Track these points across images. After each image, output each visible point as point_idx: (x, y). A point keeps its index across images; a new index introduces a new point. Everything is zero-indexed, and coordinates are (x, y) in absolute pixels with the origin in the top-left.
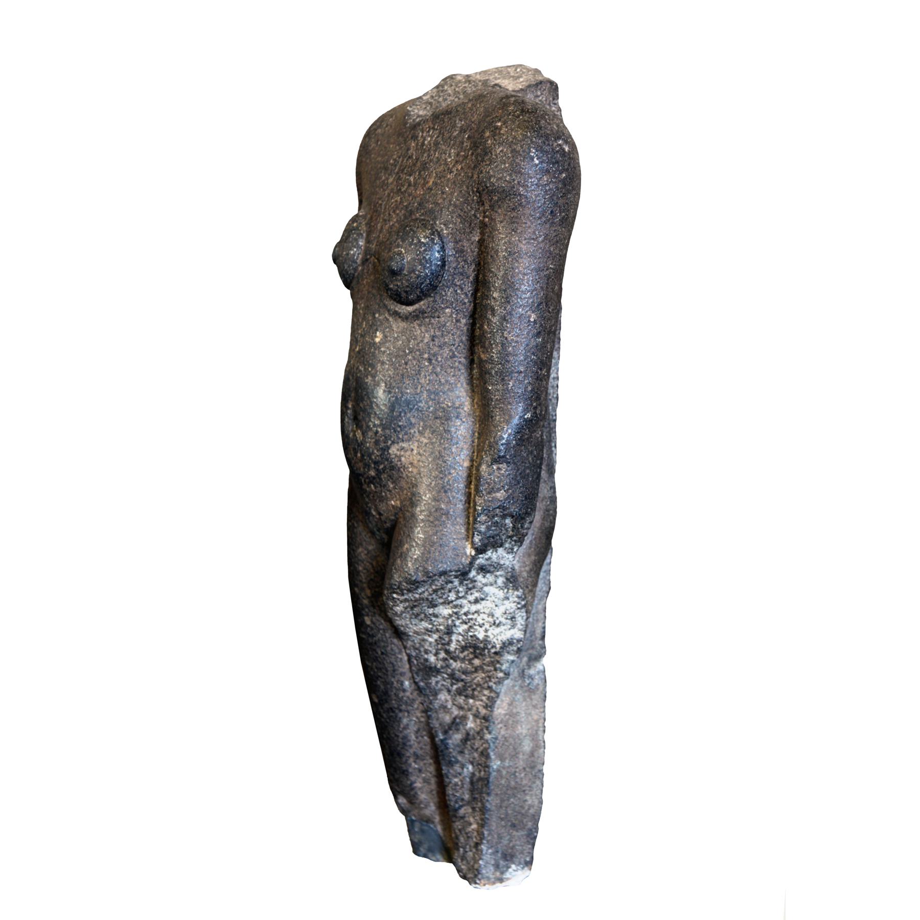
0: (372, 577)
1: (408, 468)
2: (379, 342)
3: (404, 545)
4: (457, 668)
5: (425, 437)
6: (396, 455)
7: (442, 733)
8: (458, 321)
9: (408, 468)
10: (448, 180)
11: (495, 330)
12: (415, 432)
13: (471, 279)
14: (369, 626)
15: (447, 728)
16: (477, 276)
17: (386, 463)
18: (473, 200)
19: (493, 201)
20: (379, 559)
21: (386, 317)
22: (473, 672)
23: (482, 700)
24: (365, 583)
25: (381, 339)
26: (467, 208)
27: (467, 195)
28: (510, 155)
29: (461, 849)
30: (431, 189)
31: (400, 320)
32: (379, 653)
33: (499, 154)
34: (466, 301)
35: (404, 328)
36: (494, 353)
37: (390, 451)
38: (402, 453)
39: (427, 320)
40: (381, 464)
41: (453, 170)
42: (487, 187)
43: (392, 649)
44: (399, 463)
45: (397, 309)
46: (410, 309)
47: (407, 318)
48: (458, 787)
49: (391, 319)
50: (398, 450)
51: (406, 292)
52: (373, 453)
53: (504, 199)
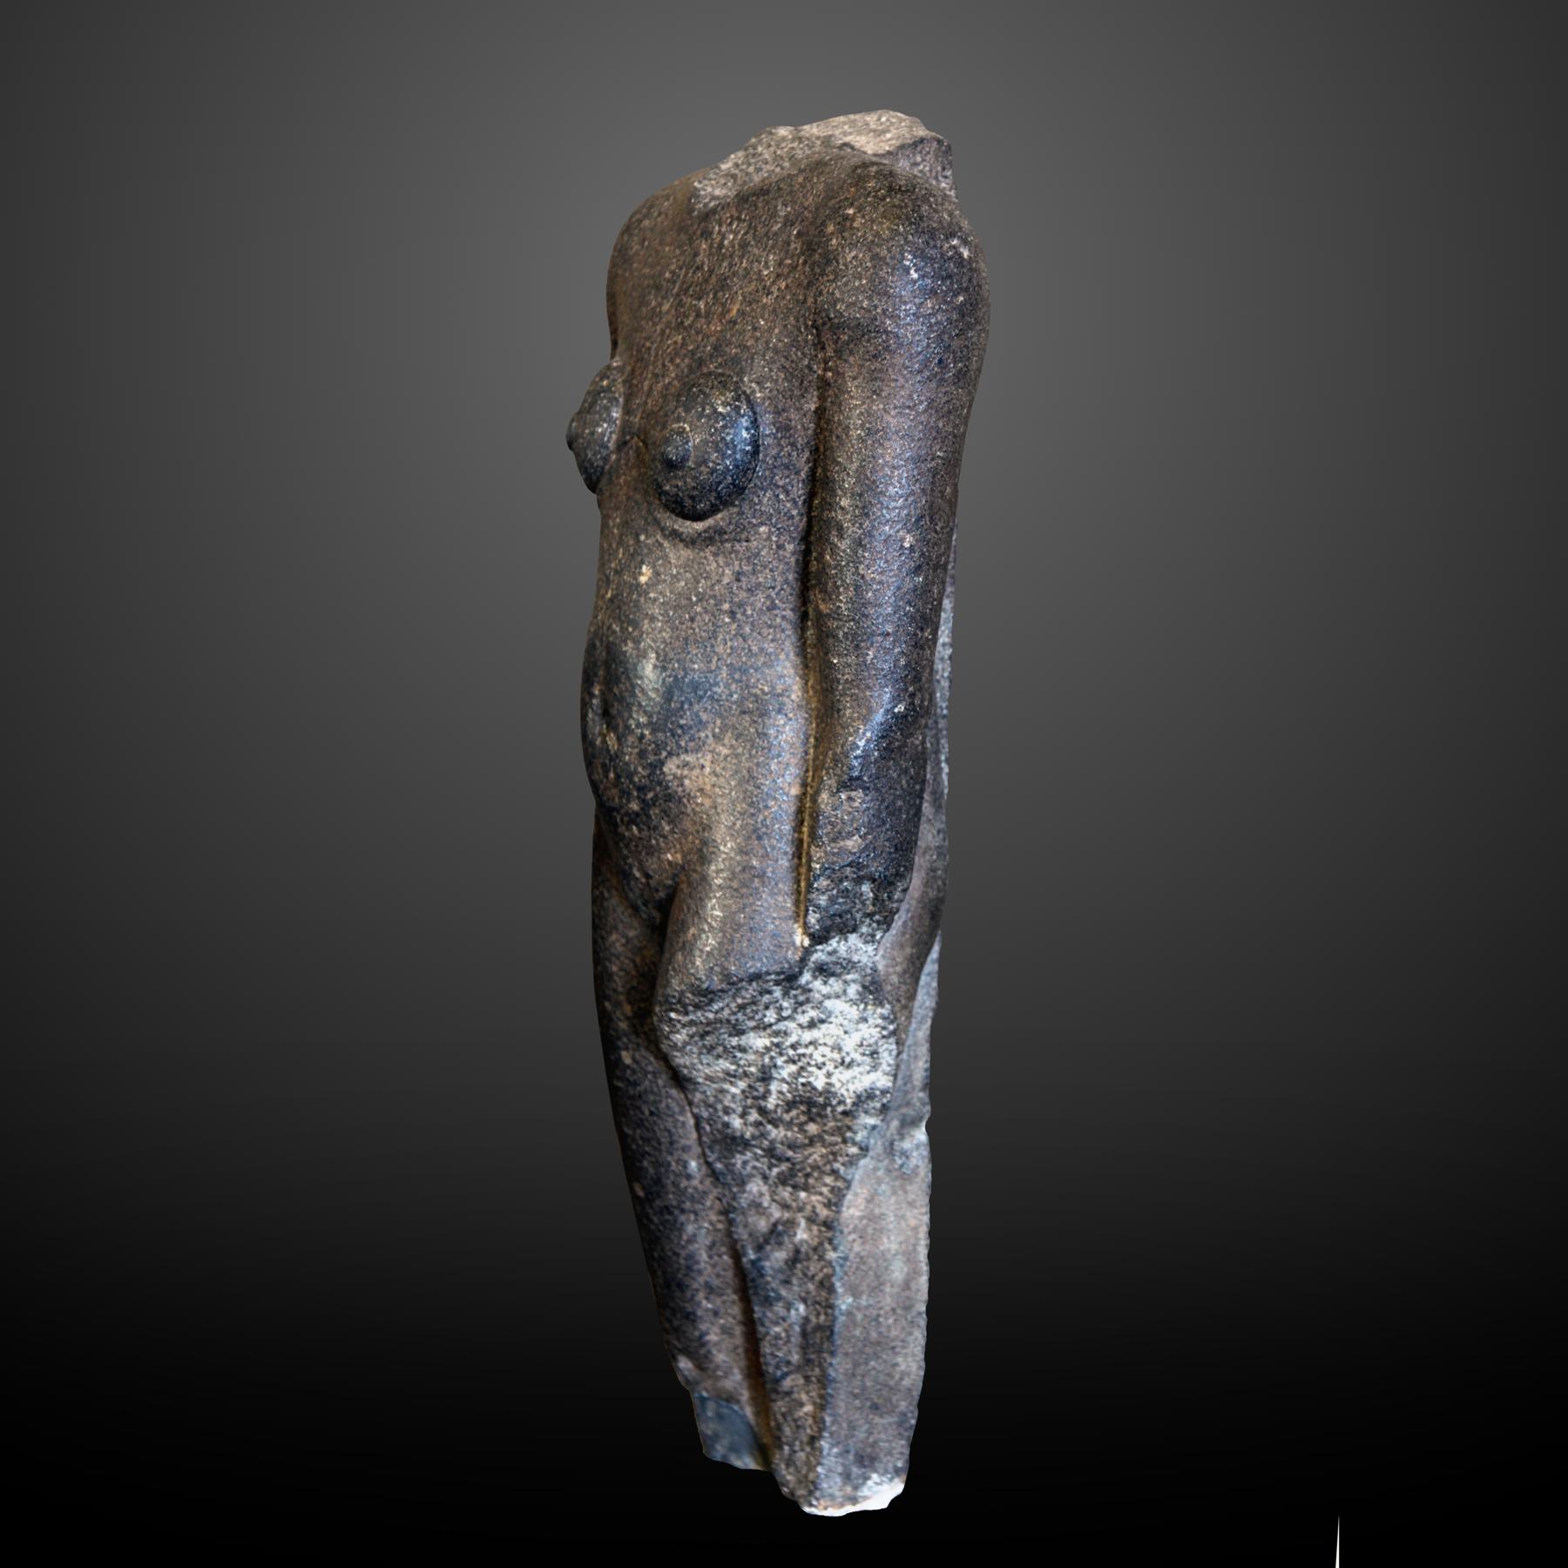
0: (635, 983)
1: (696, 797)
3: (689, 928)
4: (779, 1139)
5: (724, 745)
6: (675, 776)
7: (753, 1249)
10: (764, 307)
11: (843, 563)
12: (707, 736)
13: (803, 475)
14: (628, 1067)
15: (761, 1240)
16: (813, 471)
17: (658, 789)
18: (806, 341)
19: (840, 342)
21: (657, 541)
22: (806, 1145)
23: (821, 1194)
24: (621, 993)
25: (650, 579)
26: (796, 355)
27: (796, 332)
28: (868, 264)
29: (786, 1448)
31: (681, 545)
32: (647, 1112)
33: (851, 262)
34: (795, 512)
35: (688, 560)
36: (841, 601)
37: (665, 769)
38: (686, 772)
39: (728, 545)
40: (650, 791)
41: (773, 289)
42: (830, 319)
43: (668, 1107)
44: (680, 789)
45: (676, 527)
46: (699, 526)
47: (693, 542)
48: (780, 1342)
49: (666, 544)
50: (678, 767)
51: (692, 498)
52: (636, 772)
53: (860, 340)
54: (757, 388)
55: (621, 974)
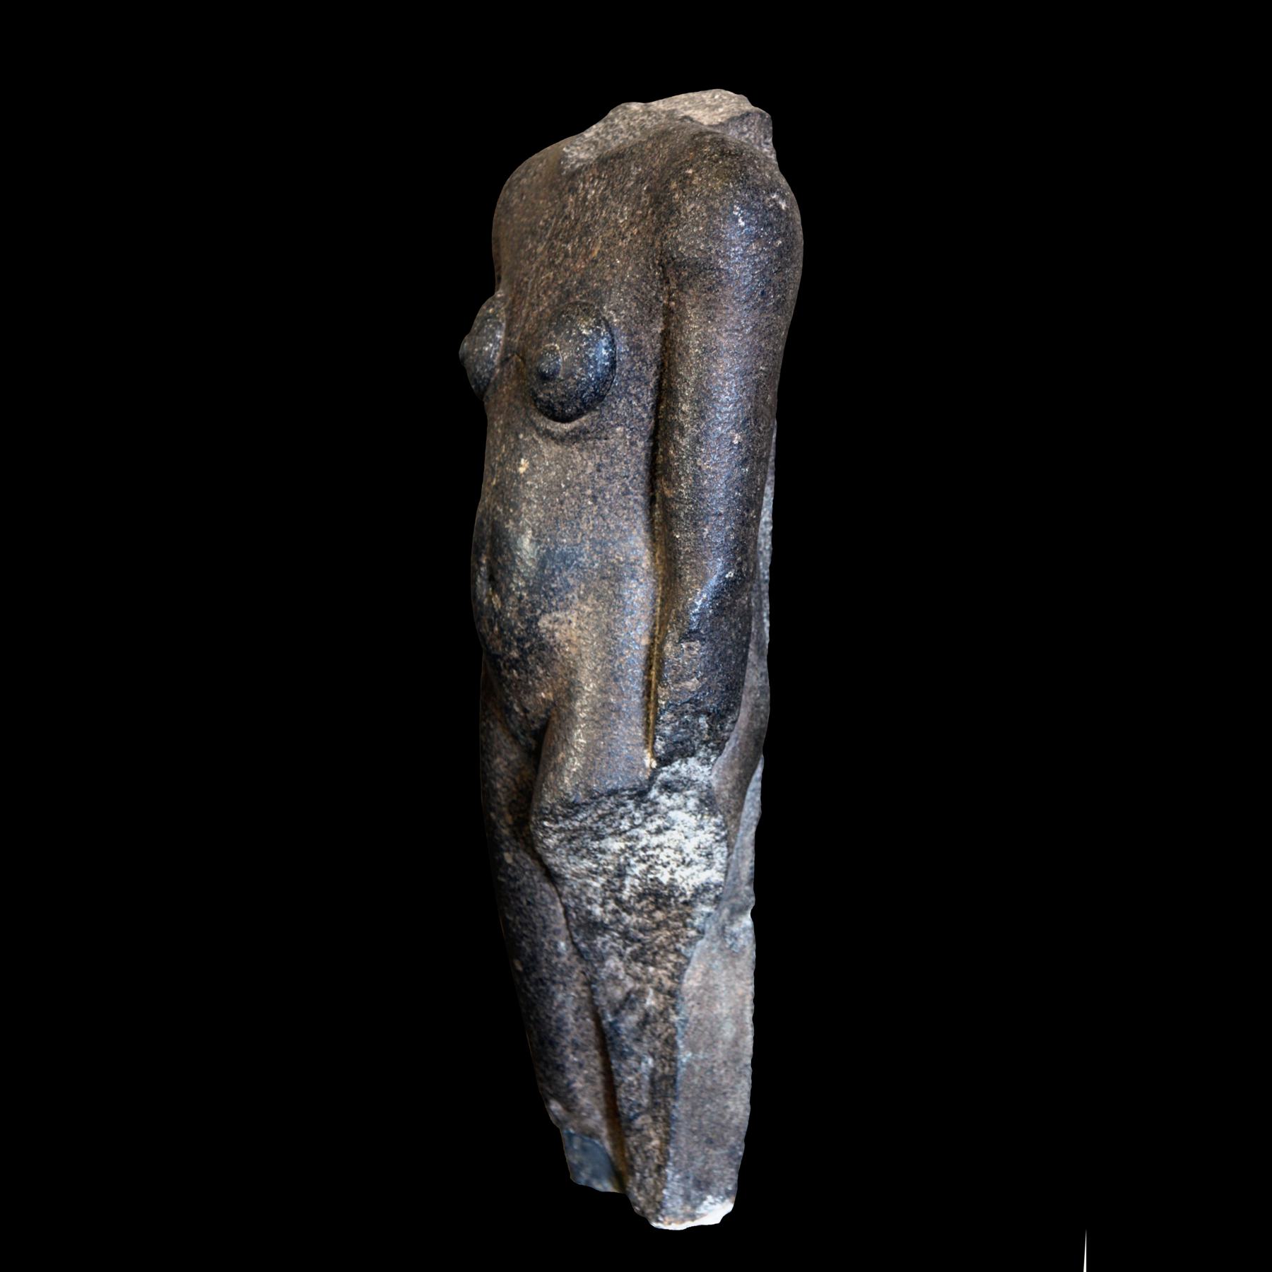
0: (515, 797)
2: (524, 473)
3: (559, 753)
4: (632, 924)
5: (587, 604)
6: (547, 629)
7: (611, 1013)
8: (633, 444)
9: (564, 646)
10: (620, 249)
11: (684, 457)
12: (573, 597)
13: (651, 385)
14: (510, 865)
15: (617, 1006)
16: (659, 382)
17: (534, 640)
18: (654, 277)
19: (681, 278)
20: (523, 773)
21: (533, 439)
22: (654, 929)
23: (666, 968)
24: (504, 806)
25: (527, 469)
26: (646, 288)
27: (646, 270)
28: (704, 214)
29: (638, 1174)
30: (596, 262)
31: (553, 442)
32: (525, 902)
33: (690, 212)
34: (645, 416)
35: (558, 454)
36: (682, 488)
37: (539, 624)
38: (556, 627)
39: (591, 442)
40: (527, 641)
41: (627, 235)
43: (542, 898)
44: (552, 640)
46: (567, 427)
47: (562, 440)
48: (633, 1089)
49: (540, 441)
50: (550, 622)
51: (562, 404)
52: (516, 626)
53: (697, 275)
54: (614, 315)
55: (504, 790)
